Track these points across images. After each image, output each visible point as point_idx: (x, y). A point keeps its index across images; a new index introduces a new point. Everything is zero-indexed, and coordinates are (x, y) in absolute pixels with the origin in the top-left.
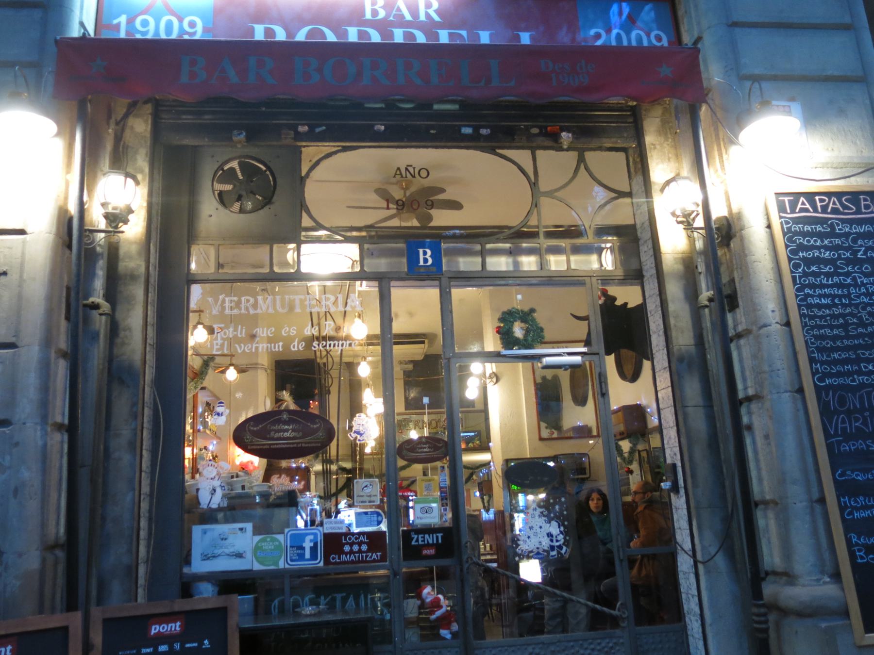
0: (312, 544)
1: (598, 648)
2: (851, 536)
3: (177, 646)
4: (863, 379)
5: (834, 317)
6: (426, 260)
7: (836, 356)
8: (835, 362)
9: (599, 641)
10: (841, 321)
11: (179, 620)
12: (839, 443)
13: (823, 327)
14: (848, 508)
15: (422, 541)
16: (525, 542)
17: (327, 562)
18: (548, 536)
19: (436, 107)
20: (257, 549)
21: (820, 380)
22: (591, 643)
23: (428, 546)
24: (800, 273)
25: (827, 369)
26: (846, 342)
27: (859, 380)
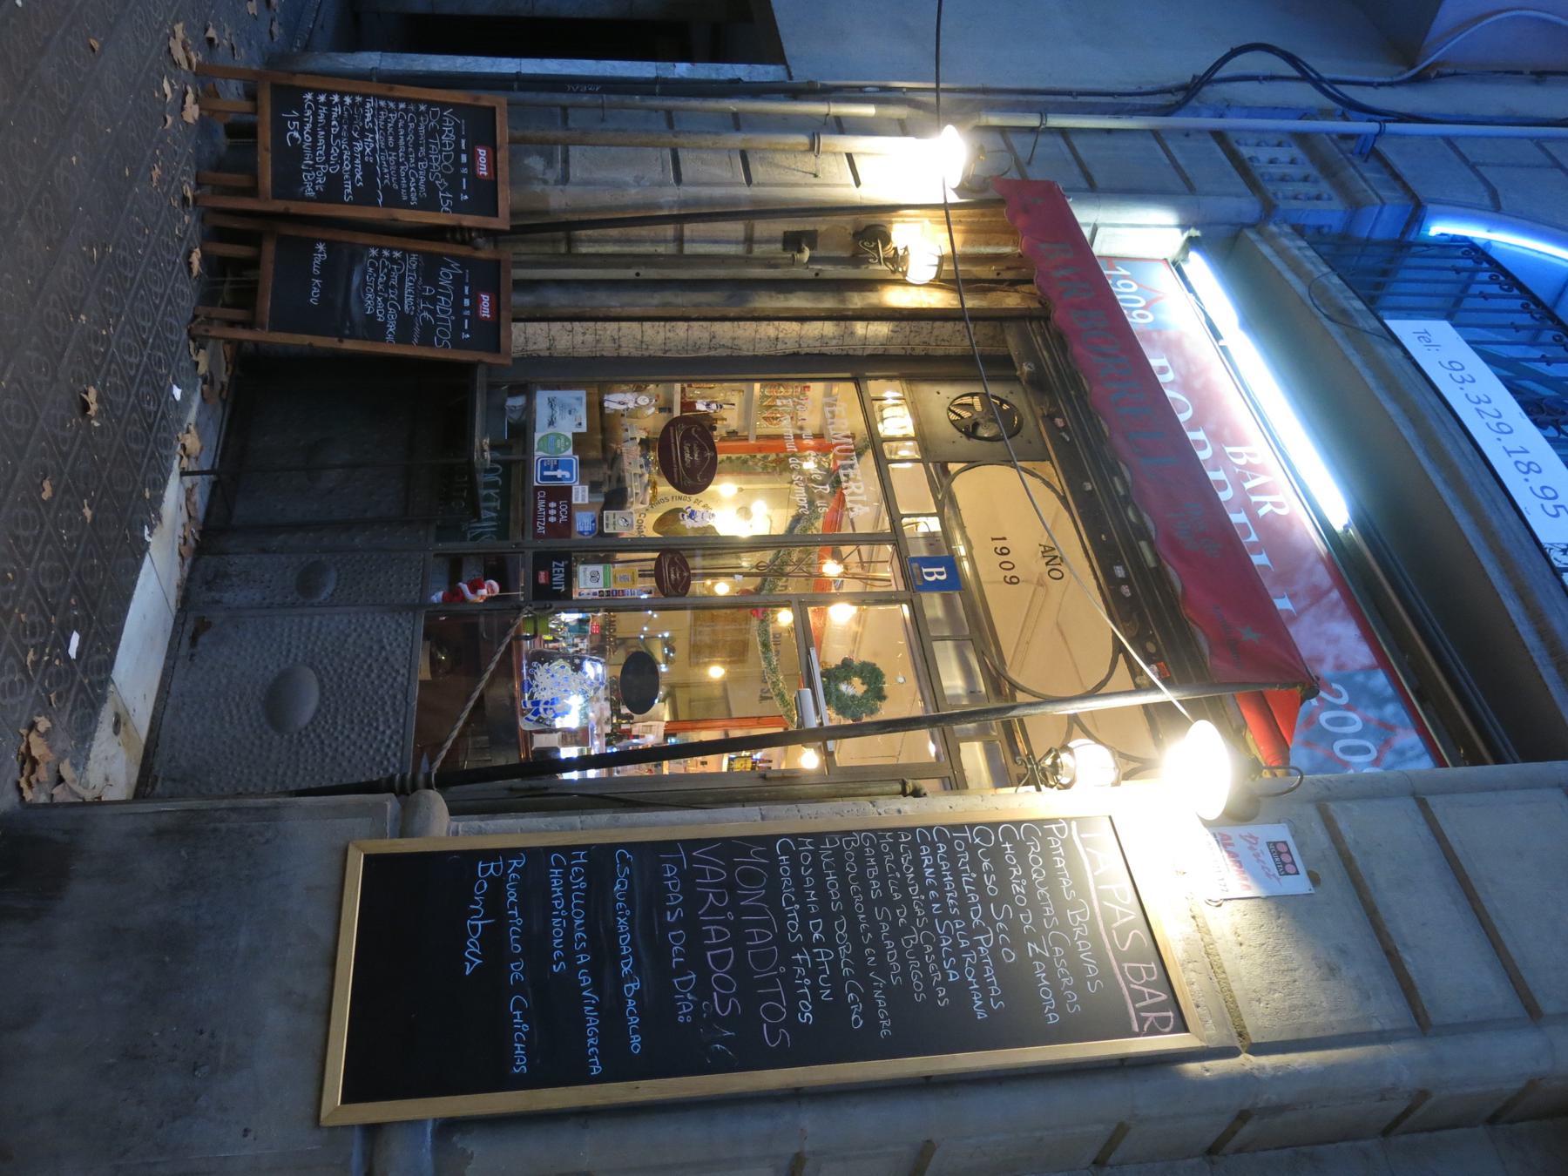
0: (559, 476)
1: (389, 754)
2: (521, 858)
3: (464, 171)
4: (793, 918)
5: (903, 886)
6: (931, 574)
7: (831, 878)
8: (819, 876)
9: (399, 754)
10: (897, 896)
11: (490, 174)
12: (679, 863)
13: (880, 863)
14: (569, 861)
15: (556, 572)
16: (548, 671)
17: (538, 489)
18: (553, 699)
19: (1143, 544)
20: (558, 436)
21: (784, 847)
22: (397, 744)
23: (550, 576)
24: (973, 840)
25: (806, 860)
26: (859, 898)
27: (791, 911)
